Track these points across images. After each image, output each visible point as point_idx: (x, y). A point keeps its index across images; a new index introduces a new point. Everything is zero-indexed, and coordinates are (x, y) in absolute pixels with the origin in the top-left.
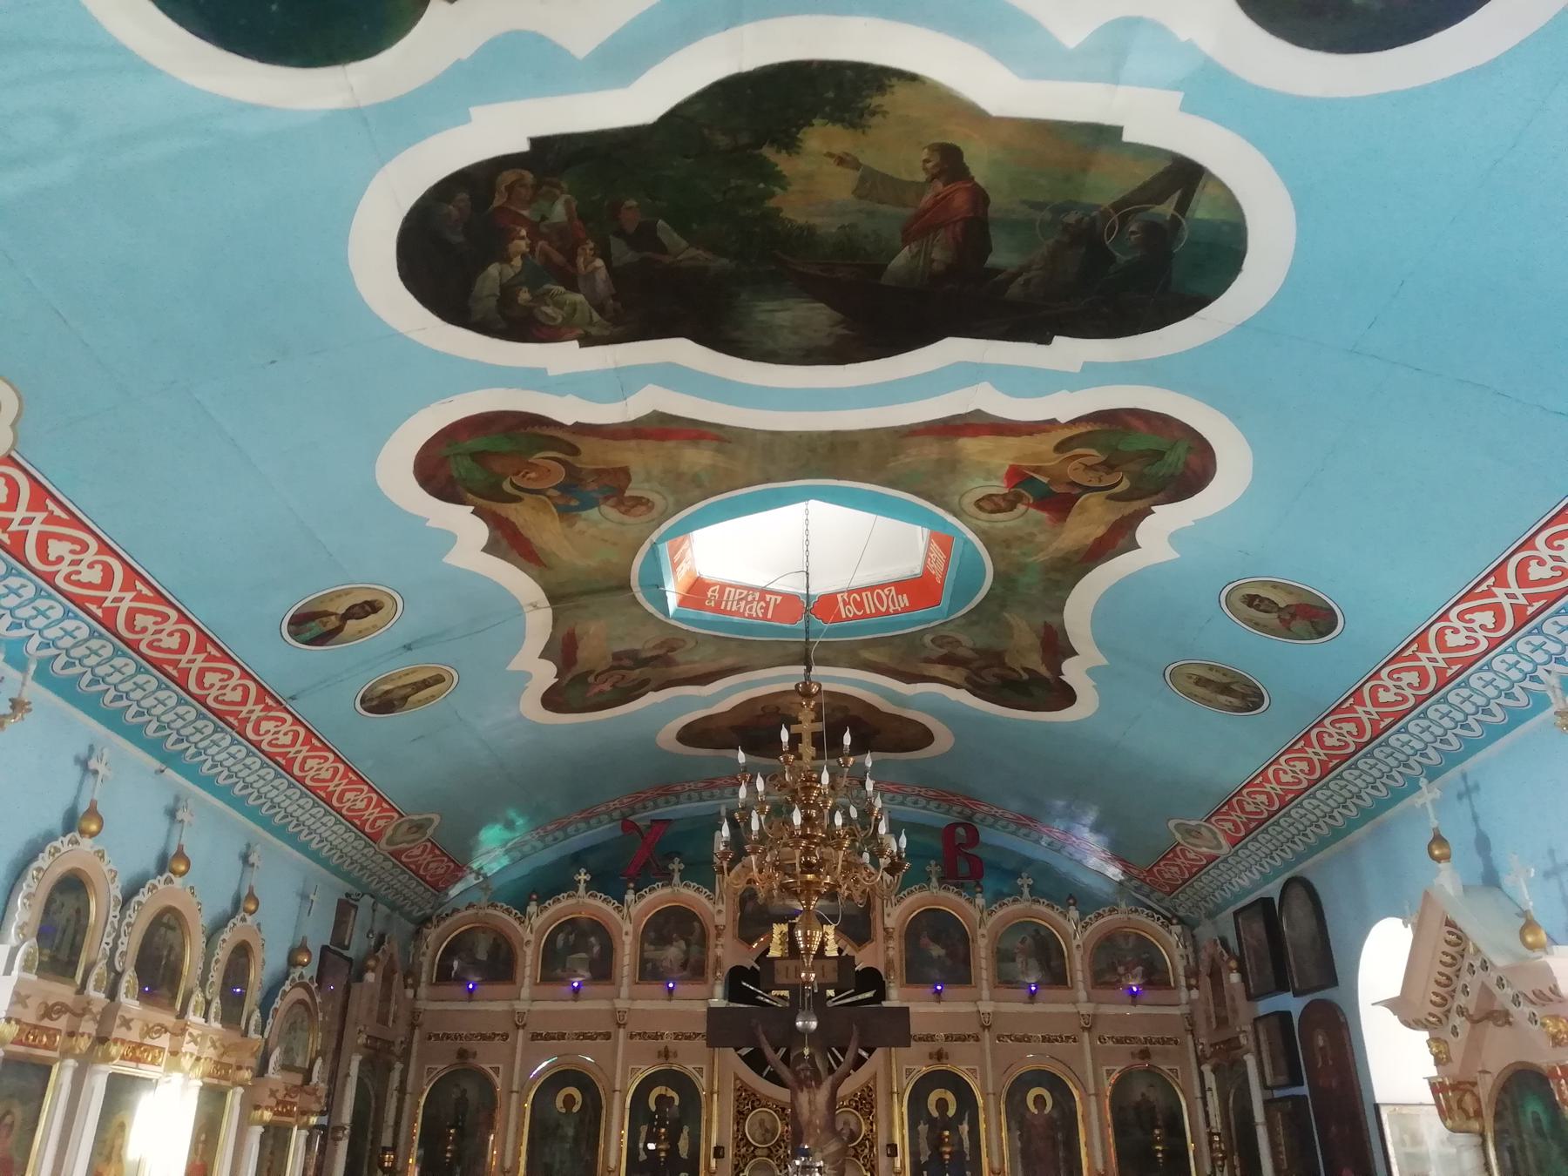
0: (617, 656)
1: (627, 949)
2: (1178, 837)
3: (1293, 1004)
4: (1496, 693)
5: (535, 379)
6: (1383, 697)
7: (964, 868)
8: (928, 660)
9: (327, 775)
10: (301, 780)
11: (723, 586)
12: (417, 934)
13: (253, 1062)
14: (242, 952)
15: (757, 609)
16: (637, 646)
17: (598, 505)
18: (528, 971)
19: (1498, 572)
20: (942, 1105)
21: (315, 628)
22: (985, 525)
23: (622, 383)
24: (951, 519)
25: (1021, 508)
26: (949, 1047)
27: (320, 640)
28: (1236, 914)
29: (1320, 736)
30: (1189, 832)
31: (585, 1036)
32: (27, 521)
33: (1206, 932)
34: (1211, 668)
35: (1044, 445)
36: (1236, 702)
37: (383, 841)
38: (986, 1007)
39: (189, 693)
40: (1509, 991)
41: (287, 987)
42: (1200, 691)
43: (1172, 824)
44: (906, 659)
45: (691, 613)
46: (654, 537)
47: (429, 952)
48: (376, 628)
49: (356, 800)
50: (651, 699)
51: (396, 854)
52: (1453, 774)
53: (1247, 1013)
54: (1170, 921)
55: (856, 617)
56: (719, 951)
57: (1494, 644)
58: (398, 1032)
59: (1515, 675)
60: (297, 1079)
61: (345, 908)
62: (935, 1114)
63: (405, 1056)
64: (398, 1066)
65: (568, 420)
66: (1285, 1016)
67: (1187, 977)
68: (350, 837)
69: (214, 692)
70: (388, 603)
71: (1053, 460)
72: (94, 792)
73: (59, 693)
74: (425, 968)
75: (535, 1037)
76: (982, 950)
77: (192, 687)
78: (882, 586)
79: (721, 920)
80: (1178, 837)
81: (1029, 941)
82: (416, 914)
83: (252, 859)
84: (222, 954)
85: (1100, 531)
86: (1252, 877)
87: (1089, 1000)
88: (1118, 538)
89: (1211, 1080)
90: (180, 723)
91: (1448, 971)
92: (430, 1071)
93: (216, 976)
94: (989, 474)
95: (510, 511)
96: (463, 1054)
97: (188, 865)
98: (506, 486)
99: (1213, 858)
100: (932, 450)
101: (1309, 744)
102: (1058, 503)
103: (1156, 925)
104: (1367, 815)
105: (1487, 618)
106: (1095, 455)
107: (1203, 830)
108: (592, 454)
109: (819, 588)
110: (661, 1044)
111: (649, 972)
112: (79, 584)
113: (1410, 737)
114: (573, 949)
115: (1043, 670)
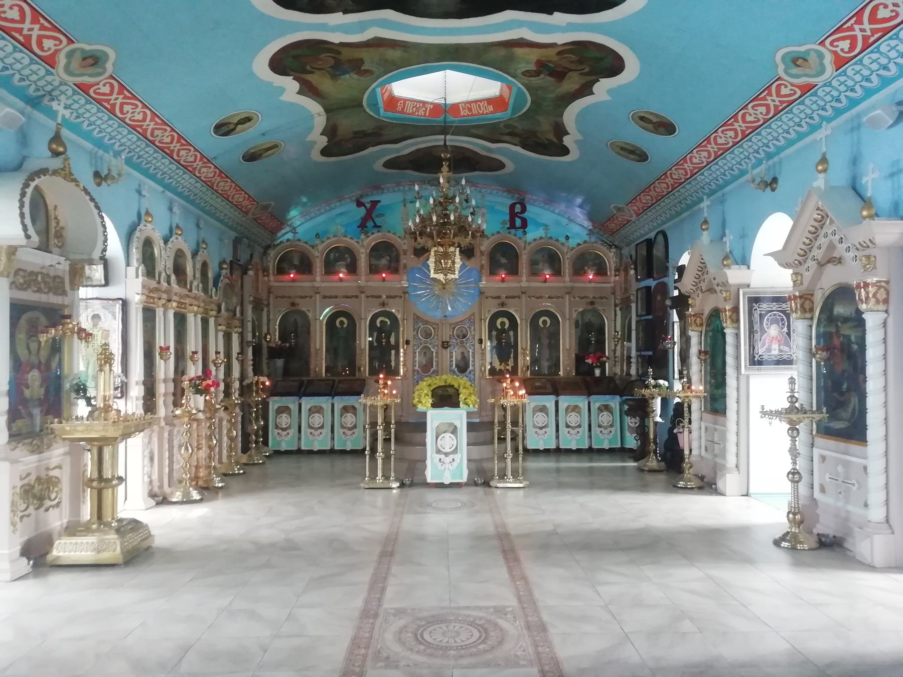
0: (355, 133)
1: (363, 260)
2: (615, 212)
3: (652, 283)
4: (845, 89)
5: (323, 27)
6: (695, 161)
7: (518, 222)
8: (502, 134)
9: (227, 188)
10: (199, 178)
11: (405, 100)
12: (265, 253)
13: (216, 308)
14: (205, 265)
15: (421, 112)
16: (365, 128)
17: (348, 73)
18: (318, 270)
19: (859, 14)
20: (503, 324)
21: (225, 129)
22: (527, 82)
23: (362, 26)
24: (510, 78)
25: (542, 76)
26: (506, 301)
27: (226, 134)
28: (637, 245)
29: (744, 116)
30: (619, 209)
31: (347, 297)
32: (116, 99)
33: (625, 251)
34: (627, 144)
35: (552, 52)
36: (638, 158)
37: (250, 215)
38: (524, 284)
39: (147, 139)
40: (844, 246)
41: (222, 278)
42: (622, 152)
43: (612, 206)
44: (493, 133)
45: (390, 114)
46: (374, 86)
47: (272, 262)
48: (250, 127)
49: (239, 198)
50: (371, 150)
51: (255, 219)
52: (719, 194)
53: (635, 286)
54: (611, 246)
55: (468, 115)
56: (405, 261)
57: (735, 144)
58: (264, 295)
59: (751, 151)
60: (231, 314)
61: (236, 242)
62: (499, 327)
63: (268, 305)
64: (265, 309)
65: (337, 41)
66: (648, 288)
67: (615, 271)
68: (236, 213)
69: (183, 158)
70: (255, 117)
71: (556, 59)
72: (145, 204)
73: (142, 174)
74: (271, 267)
75: (325, 297)
76: (524, 260)
77: (175, 157)
78: (481, 101)
79: (405, 247)
80: (615, 212)
81: (546, 256)
82: (264, 245)
83: (143, 193)
84: (199, 266)
85: (577, 87)
86: (644, 229)
87: (571, 281)
88: (586, 90)
89: (619, 313)
90: (138, 149)
91: (700, 273)
92: (279, 311)
93: (198, 275)
94: (528, 62)
95: (309, 77)
96: (293, 304)
97: (152, 217)
98: (308, 68)
99: (629, 221)
100: (503, 52)
101: (736, 121)
102: (559, 74)
103: (605, 249)
104: (689, 207)
105: (732, 134)
106: (573, 57)
107: (812, 58)
108: (346, 54)
109: (451, 100)
110: (380, 300)
111: (374, 270)
112: (134, 121)
113: (705, 177)
114: (337, 260)
115: (555, 140)
